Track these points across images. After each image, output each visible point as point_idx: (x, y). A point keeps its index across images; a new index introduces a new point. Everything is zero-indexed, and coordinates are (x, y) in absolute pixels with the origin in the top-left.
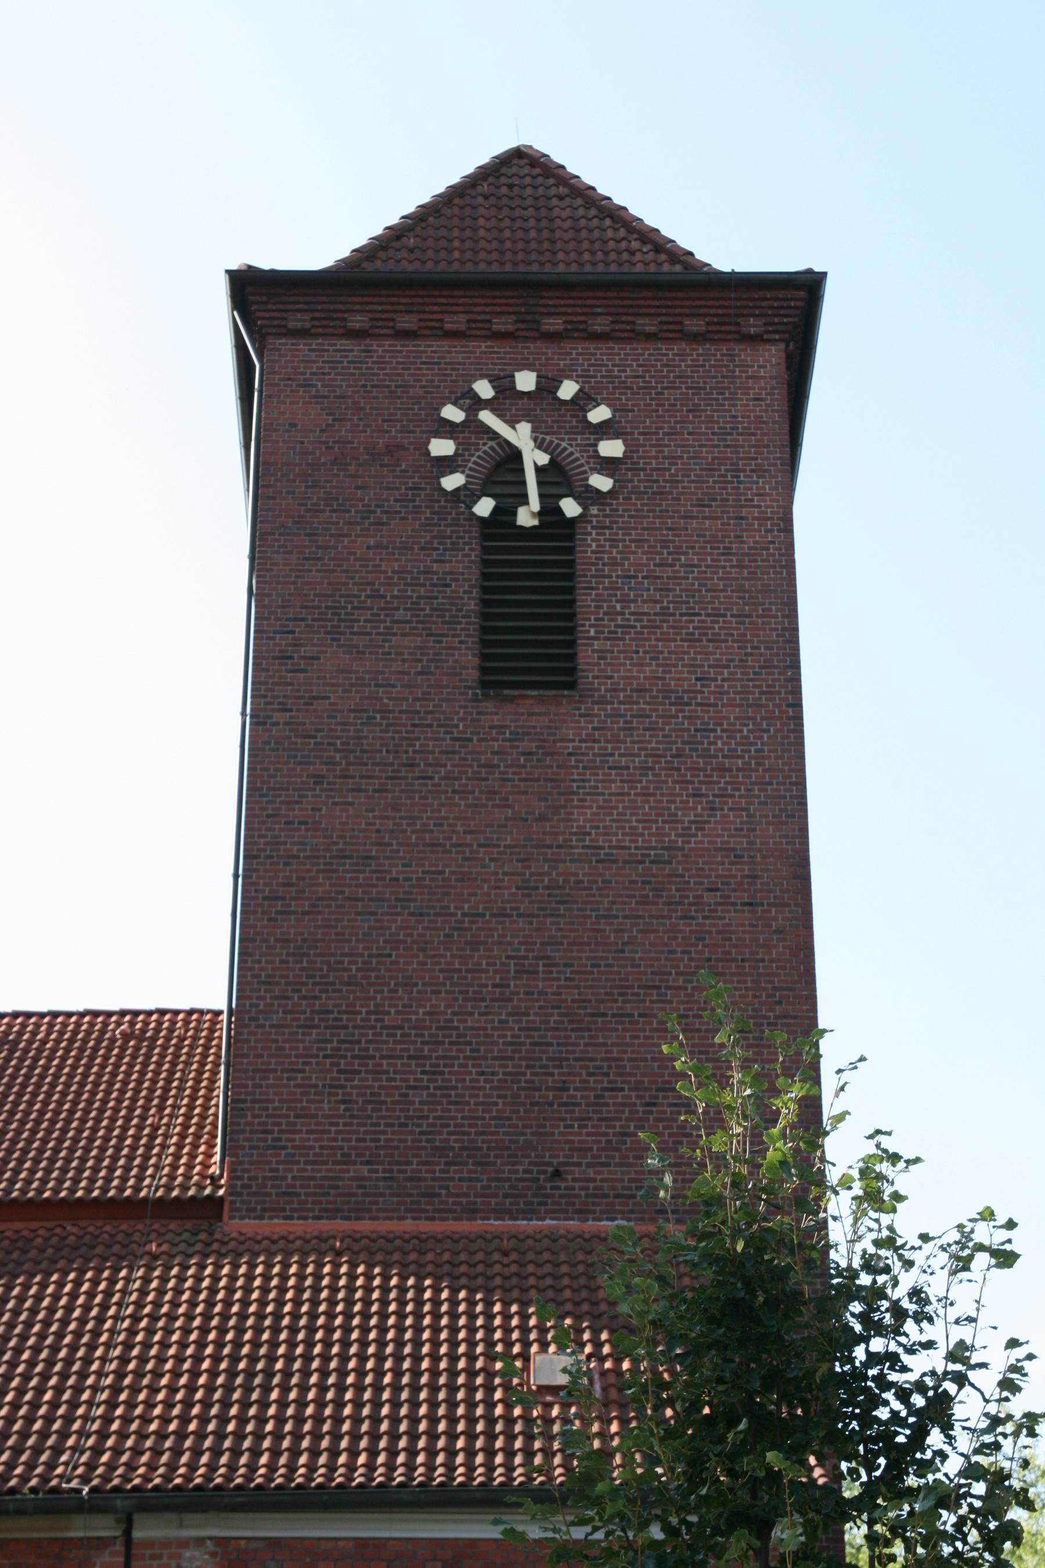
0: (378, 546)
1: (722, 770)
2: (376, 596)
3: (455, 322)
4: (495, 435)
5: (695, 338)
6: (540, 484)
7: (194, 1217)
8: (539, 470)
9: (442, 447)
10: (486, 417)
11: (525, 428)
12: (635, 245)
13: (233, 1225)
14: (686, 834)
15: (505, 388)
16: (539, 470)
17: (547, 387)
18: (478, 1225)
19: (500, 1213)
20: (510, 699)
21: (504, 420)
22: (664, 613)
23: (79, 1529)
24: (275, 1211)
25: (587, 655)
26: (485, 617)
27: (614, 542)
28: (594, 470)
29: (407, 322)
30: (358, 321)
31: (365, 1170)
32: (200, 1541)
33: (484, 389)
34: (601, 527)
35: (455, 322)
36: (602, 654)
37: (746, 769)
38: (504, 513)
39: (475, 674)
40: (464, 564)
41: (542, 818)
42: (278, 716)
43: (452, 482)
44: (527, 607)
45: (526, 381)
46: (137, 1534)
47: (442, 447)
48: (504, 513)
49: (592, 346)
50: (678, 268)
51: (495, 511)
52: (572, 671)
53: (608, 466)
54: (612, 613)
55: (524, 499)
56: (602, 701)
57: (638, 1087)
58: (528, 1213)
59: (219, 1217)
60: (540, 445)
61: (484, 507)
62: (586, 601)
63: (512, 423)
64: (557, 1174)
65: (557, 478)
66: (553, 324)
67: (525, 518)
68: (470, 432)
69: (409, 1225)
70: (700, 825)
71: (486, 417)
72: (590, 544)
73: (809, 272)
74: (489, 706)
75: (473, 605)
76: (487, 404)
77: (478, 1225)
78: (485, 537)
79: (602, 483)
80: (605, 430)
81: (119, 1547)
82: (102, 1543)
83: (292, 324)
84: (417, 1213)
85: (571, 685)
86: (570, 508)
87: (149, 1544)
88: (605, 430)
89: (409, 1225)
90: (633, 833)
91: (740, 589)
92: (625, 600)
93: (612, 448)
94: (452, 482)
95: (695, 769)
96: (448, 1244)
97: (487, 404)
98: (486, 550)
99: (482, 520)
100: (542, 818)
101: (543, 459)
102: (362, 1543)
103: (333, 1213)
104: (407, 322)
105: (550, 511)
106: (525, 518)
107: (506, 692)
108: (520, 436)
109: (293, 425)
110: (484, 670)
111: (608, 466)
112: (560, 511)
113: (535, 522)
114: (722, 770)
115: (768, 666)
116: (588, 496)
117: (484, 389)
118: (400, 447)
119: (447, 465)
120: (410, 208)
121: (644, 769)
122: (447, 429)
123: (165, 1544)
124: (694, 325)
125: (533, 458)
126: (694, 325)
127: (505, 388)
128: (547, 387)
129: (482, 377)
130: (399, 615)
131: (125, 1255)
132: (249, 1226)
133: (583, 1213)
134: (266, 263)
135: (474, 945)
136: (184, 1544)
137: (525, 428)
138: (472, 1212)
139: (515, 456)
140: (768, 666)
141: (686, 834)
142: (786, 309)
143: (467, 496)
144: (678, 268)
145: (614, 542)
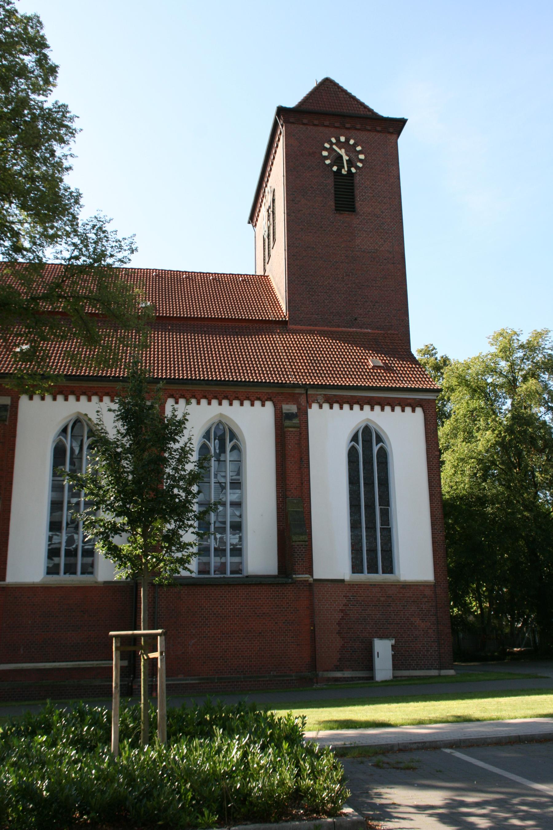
0: (312, 176)
1: (387, 233)
2: (312, 187)
3: (327, 123)
4: (336, 151)
5: (379, 132)
6: (347, 164)
7: (280, 326)
8: (347, 161)
9: (325, 153)
10: (334, 147)
11: (343, 150)
12: (360, 106)
13: (291, 326)
14: (379, 247)
15: (338, 140)
16: (347, 161)
17: (347, 141)
18: (340, 329)
19: (344, 327)
20: (342, 214)
21: (339, 148)
22: (373, 196)
23: (297, 391)
24: (299, 324)
25: (358, 204)
26: (335, 194)
27: (362, 179)
28: (358, 162)
29: (316, 122)
30: (305, 121)
31: (316, 316)
32: (321, 394)
33: (333, 140)
34: (359, 175)
35: (327, 123)
36: (361, 205)
37: (391, 233)
38: (339, 170)
39: (334, 207)
40: (330, 181)
41: (350, 241)
42: (292, 214)
43: (328, 162)
44: (344, 193)
45: (343, 139)
46: (309, 392)
47: (325, 153)
48: (339, 170)
49: (356, 132)
50: (370, 113)
51: (337, 169)
52: (354, 208)
53: (361, 161)
54: (362, 195)
55: (343, 167)
56: (361, 216)
57: (371, 302)
58: (350, 327)
59: (287, 324)
60: (347, 155)
61: (335, 168)
62: (357, 192)
63: (340, 149)
64: (356, 319)
65: (350, 163)
66: (348, 125)
67: (344, 172)
68: (331, 150)
69: (326, 328)
70: (382, 245)
71: (334, 147)
72: (357, 179)
73: (403, 118)
74: (337, 215)
75: (333, 191)
76: (334, 144)
77: (340, 329)
78: (334, 175)
79: (360, 165)
80: (360, 152)
81: (305, 395)
82: (301, 394)
83: (291, 121)
84: (327, 326)
85: (354, 211)
86: (353, 170)
87: (311, 394)
88: (360, 152)
89: (326, 328)
90: (369, 246)
91: (389, 192)
92: (365, 192)
93: (362, 157)
94: (328, 162)
95: (381, 232)
96: (343, 334)
97: (334, 144)
98: (335, 178)
99: (334, 172)
100: (350, 241)
101: (347, 158)
102: (351, 396)
103: (310, 325)
104: (316, 122)
105: (349, 171)
106: (344, 172)
107: (342, 212)
108: (342, 152)
109: (292, 145)
110: (336, 207)
111: (361, 161)
112: (351, 171)
113: (346, 173)
114: (387, 233)
115: (395, 210)
116: (357, 168)
117: (333, 140)
118: (315, 152)
119: (326, 158)
120: (307, 93)
121: (371, 232)
122: (326, 149)
123: (314, 395)
124: (379, 129)
125: (345, 158)
126: (379, 129)
127: (338, 140)
128: (347, 141)
129: (333, 137)
130: (317, 192)
131: (272, 333)
132: (294, 327)
133: (361, 328)
134: (284, 105)
135: (337, 269)
136: (318, 395)
137: (343, 150)
138: (339, 326)
139: (341, 157)
140: (395, 210)
141: (379, 247)
142: (397, 125)
143: (331, 165)
144: (370, 113)
145: (362, 179)
